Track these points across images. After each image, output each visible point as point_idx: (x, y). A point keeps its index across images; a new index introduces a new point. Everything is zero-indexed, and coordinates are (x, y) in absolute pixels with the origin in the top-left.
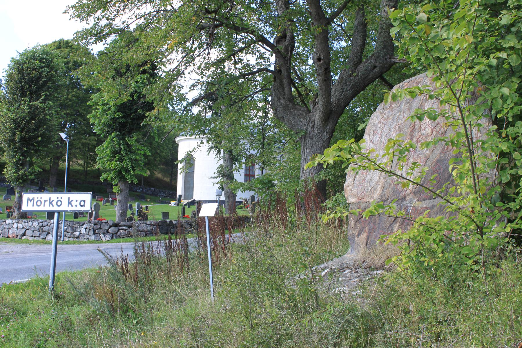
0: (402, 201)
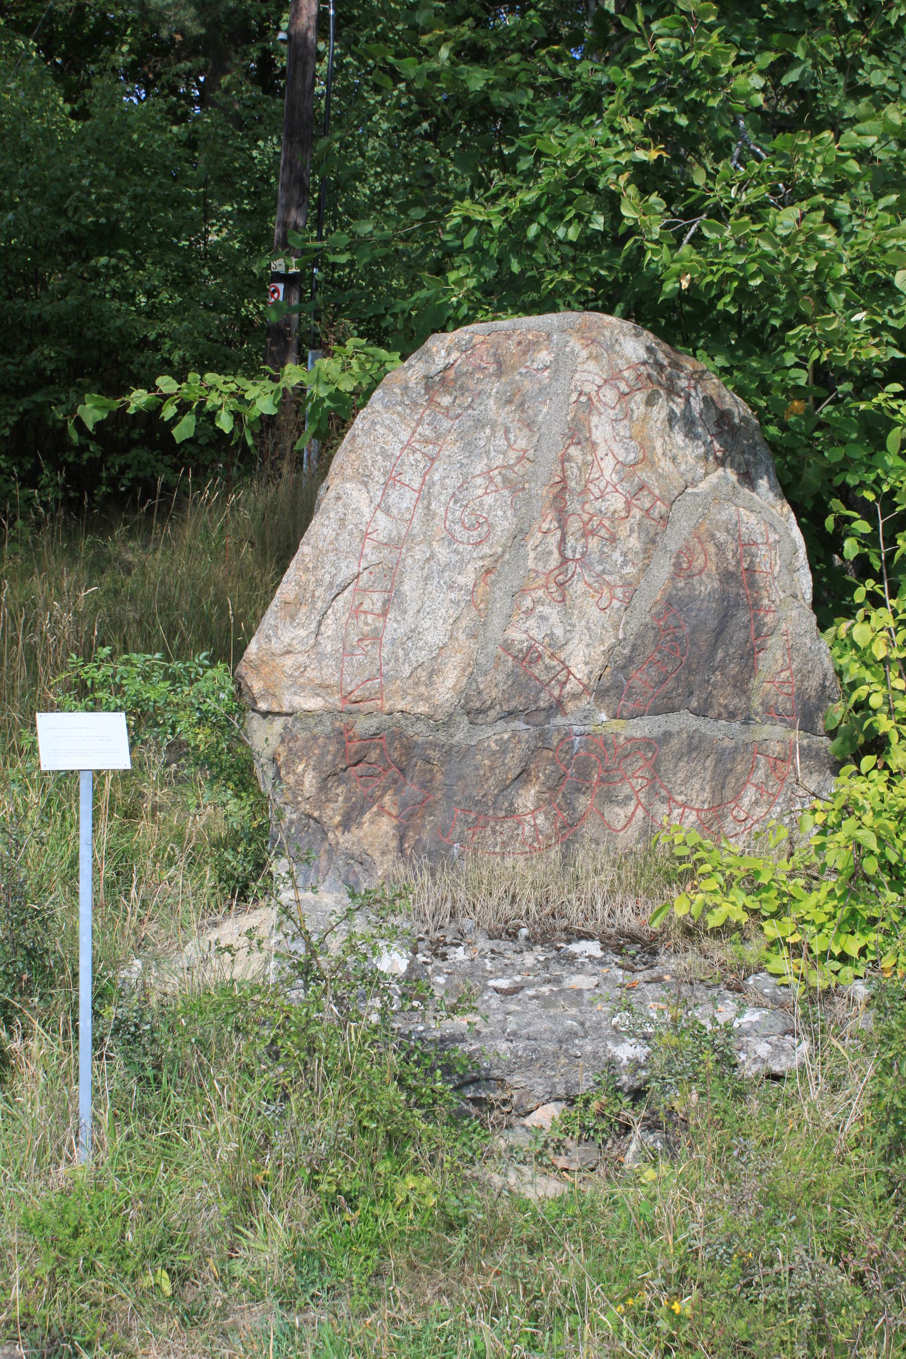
0: (548, 717)
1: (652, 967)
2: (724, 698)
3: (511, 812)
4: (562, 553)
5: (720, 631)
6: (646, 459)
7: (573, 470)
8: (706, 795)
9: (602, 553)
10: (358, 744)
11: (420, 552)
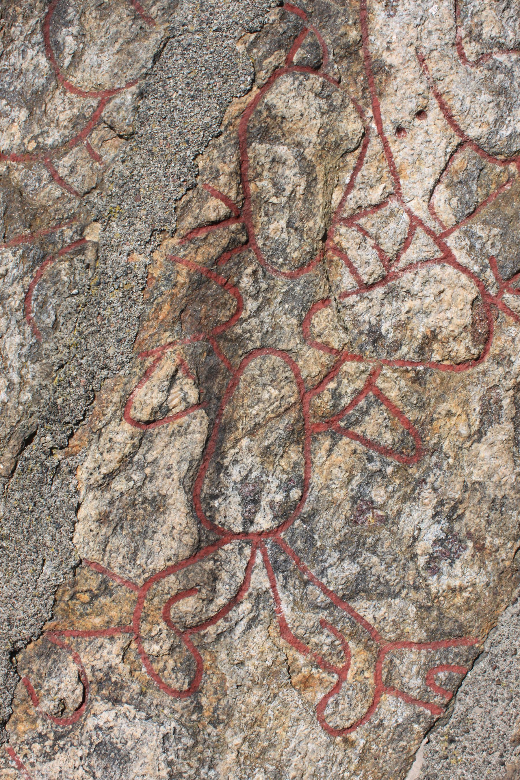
4: (201, 509)
7: (279, 168)
9: (362, 504)
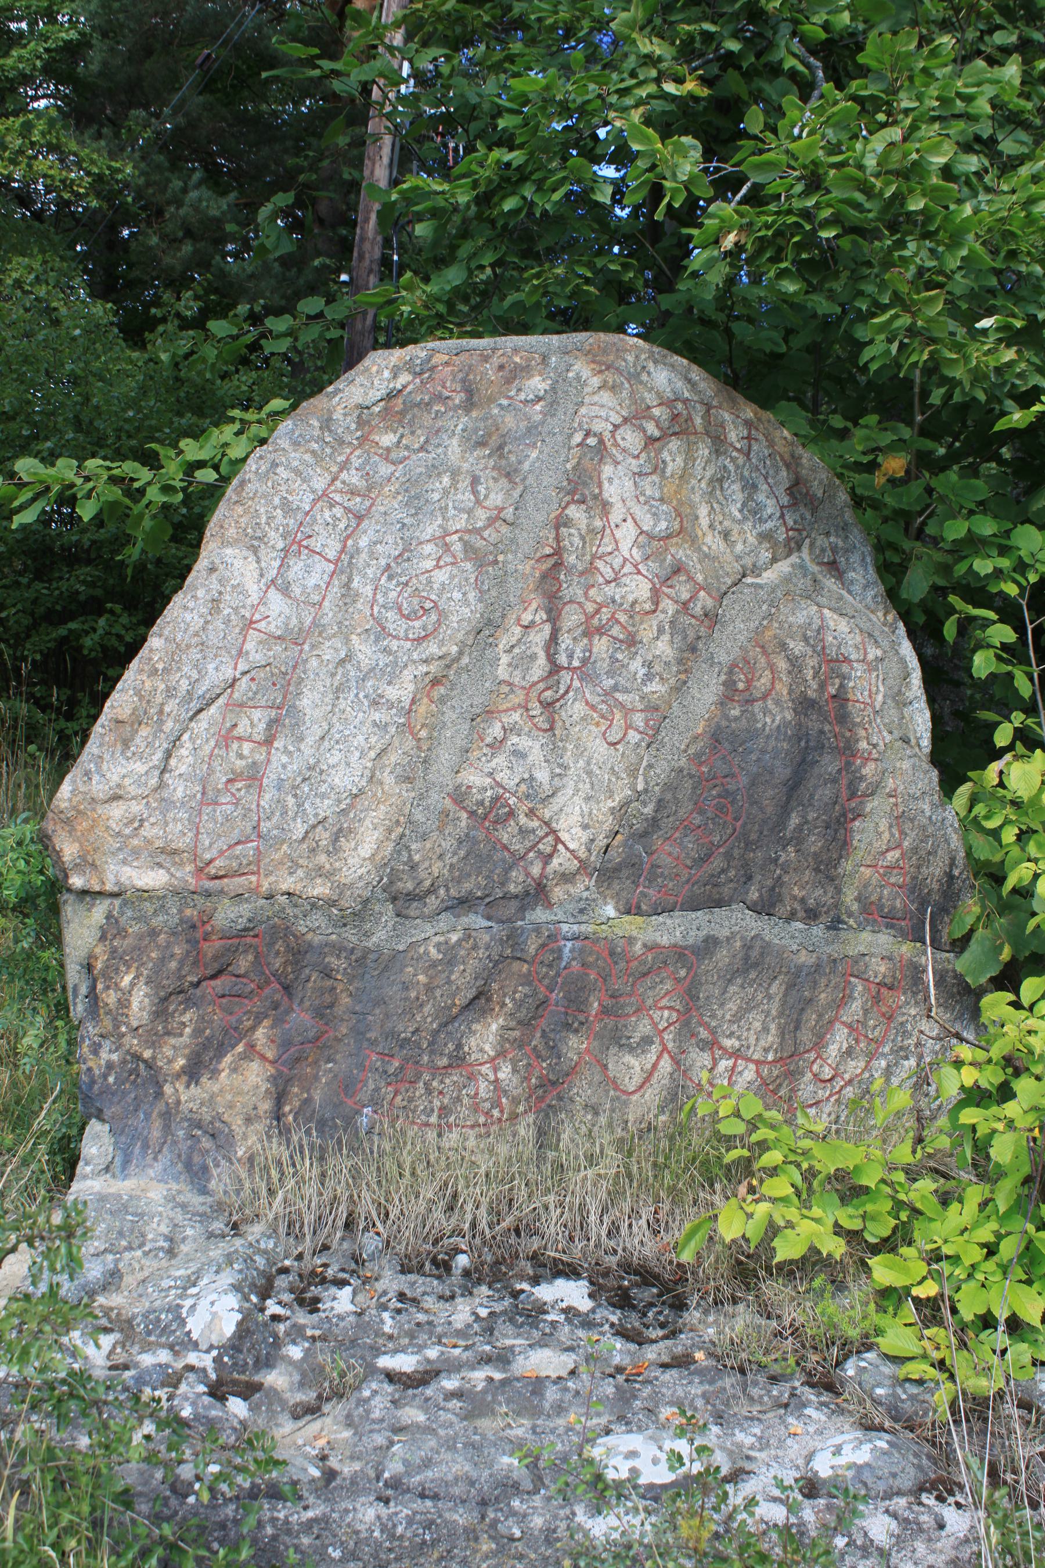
0: (523, 909)
1: (673, 1334)
2: (800, 888)
3: (458, 1060)
4: (551, 658)
5: (794, 785)
6: (684, 530)
7: (572, 539)
8: (771, 1038)
9: (614, 660)
10: (218, 944)
11: (330, 651)
